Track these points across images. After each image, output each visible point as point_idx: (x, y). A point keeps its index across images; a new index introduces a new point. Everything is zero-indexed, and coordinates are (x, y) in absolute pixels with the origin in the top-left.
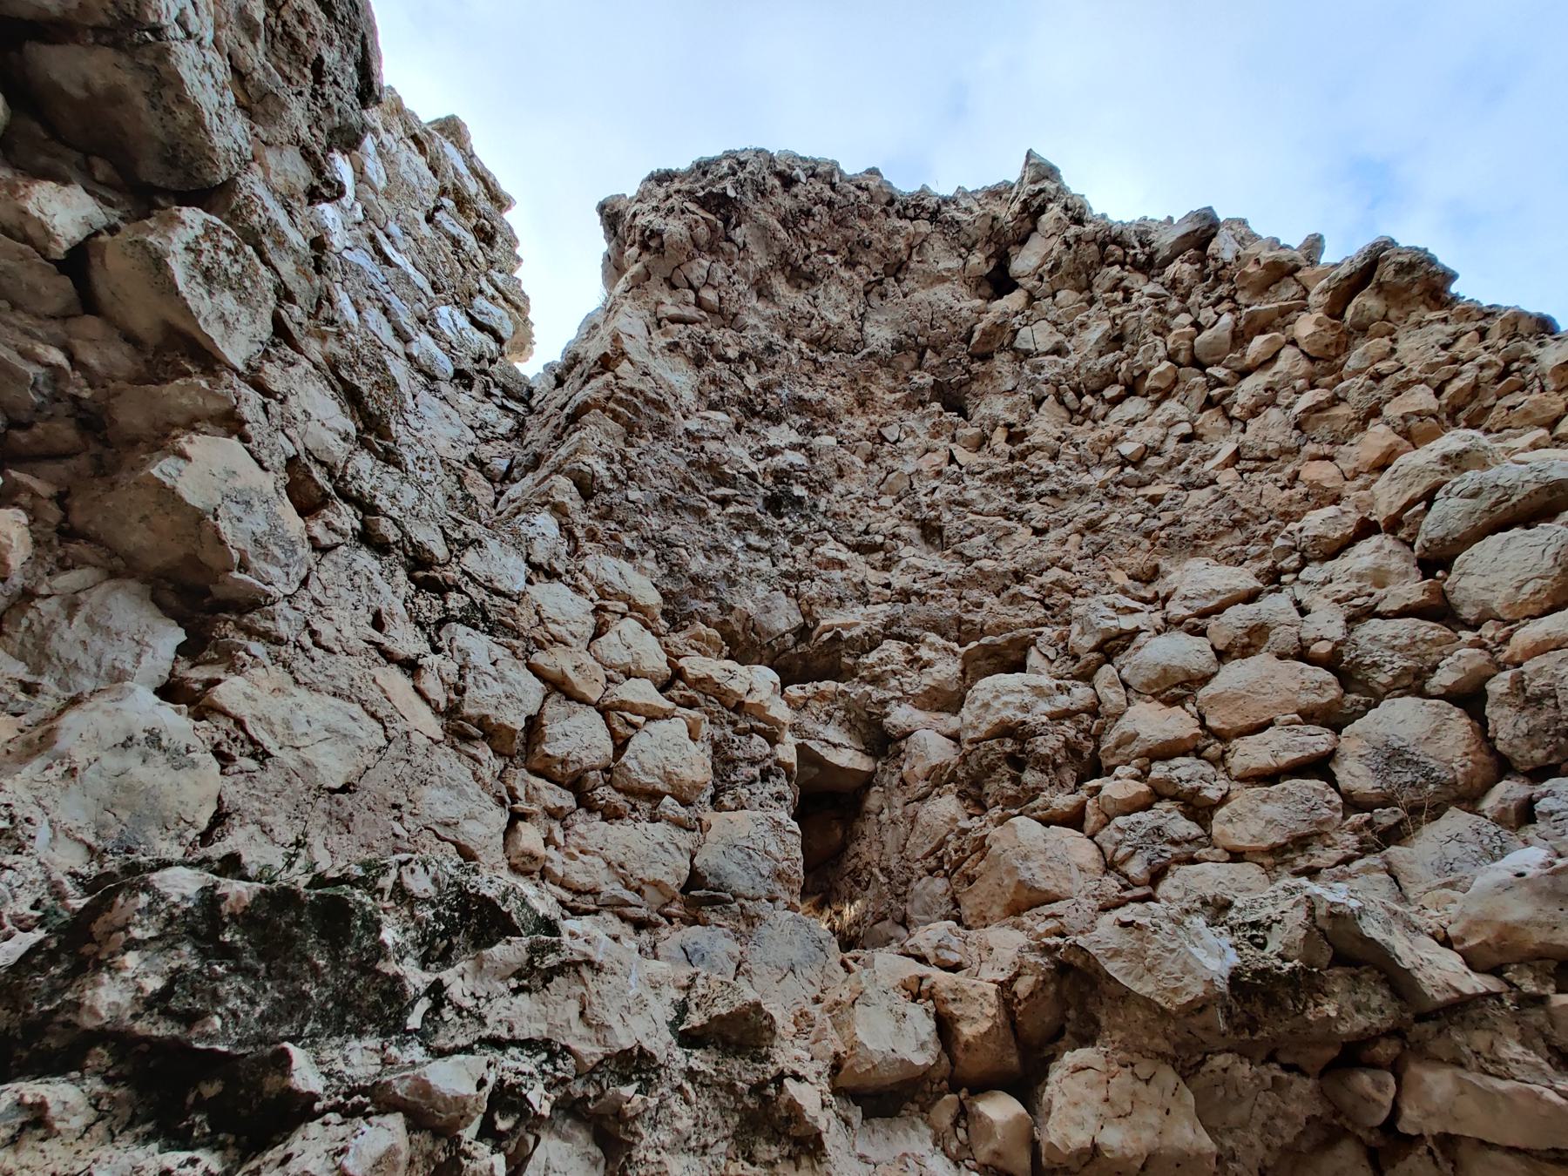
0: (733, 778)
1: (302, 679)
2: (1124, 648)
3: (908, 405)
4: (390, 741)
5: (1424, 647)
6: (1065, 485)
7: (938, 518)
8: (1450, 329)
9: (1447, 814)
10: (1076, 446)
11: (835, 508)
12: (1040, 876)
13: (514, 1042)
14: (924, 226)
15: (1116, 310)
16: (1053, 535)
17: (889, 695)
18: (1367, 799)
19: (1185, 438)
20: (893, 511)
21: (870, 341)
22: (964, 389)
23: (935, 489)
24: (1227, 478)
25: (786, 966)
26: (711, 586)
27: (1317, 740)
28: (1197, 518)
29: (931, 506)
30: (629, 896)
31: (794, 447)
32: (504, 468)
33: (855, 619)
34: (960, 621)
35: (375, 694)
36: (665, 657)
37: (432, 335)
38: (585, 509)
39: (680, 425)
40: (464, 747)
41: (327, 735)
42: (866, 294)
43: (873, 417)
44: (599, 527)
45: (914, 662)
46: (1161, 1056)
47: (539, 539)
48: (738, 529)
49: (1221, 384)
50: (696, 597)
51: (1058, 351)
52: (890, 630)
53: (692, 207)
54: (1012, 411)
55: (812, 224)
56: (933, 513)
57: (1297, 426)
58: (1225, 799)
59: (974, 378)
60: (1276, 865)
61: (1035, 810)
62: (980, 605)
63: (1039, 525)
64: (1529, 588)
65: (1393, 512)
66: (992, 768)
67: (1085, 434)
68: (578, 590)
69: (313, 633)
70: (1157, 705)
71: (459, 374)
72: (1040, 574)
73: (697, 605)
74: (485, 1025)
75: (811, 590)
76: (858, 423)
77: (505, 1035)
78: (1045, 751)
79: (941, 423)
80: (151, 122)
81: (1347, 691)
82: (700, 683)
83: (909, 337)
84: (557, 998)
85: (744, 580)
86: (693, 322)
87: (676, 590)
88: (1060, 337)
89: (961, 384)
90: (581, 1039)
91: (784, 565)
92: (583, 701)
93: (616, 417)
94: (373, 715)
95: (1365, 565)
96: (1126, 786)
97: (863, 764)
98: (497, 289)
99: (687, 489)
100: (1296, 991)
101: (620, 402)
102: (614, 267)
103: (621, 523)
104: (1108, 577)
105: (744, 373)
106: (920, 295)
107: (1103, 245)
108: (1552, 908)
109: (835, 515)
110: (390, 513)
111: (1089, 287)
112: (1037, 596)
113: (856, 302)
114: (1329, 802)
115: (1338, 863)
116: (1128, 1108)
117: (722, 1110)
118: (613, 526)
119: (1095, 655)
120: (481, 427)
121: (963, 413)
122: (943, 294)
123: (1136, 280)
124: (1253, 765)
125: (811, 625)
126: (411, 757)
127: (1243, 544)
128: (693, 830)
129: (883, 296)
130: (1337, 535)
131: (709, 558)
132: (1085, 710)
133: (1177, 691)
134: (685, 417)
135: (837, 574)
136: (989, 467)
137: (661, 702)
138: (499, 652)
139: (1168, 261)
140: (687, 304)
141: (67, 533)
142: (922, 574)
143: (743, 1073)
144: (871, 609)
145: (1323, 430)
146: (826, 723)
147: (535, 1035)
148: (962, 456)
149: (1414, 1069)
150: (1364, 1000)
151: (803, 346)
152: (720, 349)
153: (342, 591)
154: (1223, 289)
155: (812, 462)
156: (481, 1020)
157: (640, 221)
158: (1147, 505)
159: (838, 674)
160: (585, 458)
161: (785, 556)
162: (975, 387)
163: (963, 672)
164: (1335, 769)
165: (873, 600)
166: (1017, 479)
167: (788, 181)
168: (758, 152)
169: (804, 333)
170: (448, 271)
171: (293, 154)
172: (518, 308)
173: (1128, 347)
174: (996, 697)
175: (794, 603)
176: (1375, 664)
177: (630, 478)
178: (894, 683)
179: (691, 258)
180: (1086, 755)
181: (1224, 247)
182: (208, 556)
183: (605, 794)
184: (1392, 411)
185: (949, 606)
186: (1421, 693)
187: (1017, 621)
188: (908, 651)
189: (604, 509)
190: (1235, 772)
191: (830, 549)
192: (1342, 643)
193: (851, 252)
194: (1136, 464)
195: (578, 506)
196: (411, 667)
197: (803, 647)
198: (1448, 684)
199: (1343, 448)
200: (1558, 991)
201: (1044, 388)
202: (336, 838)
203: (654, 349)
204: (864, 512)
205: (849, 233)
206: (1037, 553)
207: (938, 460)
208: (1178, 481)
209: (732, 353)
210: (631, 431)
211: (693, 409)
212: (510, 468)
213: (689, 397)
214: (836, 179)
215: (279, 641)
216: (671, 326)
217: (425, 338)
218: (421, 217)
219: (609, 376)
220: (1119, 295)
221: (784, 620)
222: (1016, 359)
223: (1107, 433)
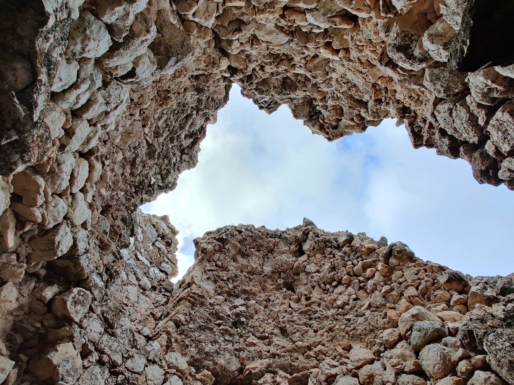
2: (333, 381)
6: (322, 315)
7: (285, 327)
8: (416, 269)
10: (325, 301)
14: (277, 240)
15: (332, 260)
16: (319, 333)
19: (355, 300)
23: (285, 316)
24: (368, 313)
26: (211, 356)
28: (361, 328)
29: (283, 322)
31: (242, 305)
32: (160, 316)
34: (291, 365)
37: (147, 277)
42: (263, 258)
43: (267, 294)
44: (179, 338)
48: (222, 334)
49: (363, 282)
50: (206, 360)
51: (318, 271)
52: (269, 369)
53: (214, 241)
54: (306, 290)
55: (247, 242)
56: (284, 325)
59: (295, 280)
62: (297, 359)
63: (315, 329)
64: (436, 367)
67: (328, 298)
68: (161, 367)
72: (315, 347)
73: (206, 363)
79: (286, 295)
80: (73, 271)
85: (222, 352)
86: (214, 271)
88: (318, 268)
89: (292, 282)
91: (236, 346)
98: (169, 259)
99: (208, 322)
101: (191, 297)
102: (197, 255)
103: (186, 336)
104: (335, 349)
105: (229, 283)
106: (278, 258)
107: (325, 243)
109: (254, 327)
111: (324, 253)
112: (314, 356)
113: (260, 261)
118: (183, 337)
120: (156, 303)
122: (284, 257)
123: (336, 252)
125: (243, 367)
127: (374, 338)
129: (268, 258)
130: (392, 340)
131: (213, 345)
134: (210, 299)
135: (252, 348)
136: (300, 309)
139: (343, 246)
141: (26, 372)
144: (263, 361)
148: (293, 305)
151: (246, 274)
154: (358, 254)
157: (202, 246)
158: (346, 322)
161: (237, 342)
162: (296, 283)
165: (264, 357)
167: (240, 232)
168: (232, 226)
171: (111, 255)
172: (174, 264)
173: (337, 270)
175: (238, 359)
177: (191, 320)
179: (214, 254)
181: (356, 243)
182: (54, 377)
184: (406, 294)
185: (286, 360)
187: (309, 365)
191: (252, 339)
193: (258, 247)
194: (342, 308)
195: (174, 331)
197: (241, 376)
201: (314, 283)
203: (203, 279)
205: (257, 243)
206: (314, 339)
209: (225, 278)
210: (193, 305)
211: (213, 296)
212: (161, 315)
213: (212, 292)
214: (253, 230)
216: (208, 273)
217: (145, 279)
218: (150, 245)
219: (189, 289)
220: (332, 256)
221: (234, 366)
222: (306, 274)
223: (333, 297)
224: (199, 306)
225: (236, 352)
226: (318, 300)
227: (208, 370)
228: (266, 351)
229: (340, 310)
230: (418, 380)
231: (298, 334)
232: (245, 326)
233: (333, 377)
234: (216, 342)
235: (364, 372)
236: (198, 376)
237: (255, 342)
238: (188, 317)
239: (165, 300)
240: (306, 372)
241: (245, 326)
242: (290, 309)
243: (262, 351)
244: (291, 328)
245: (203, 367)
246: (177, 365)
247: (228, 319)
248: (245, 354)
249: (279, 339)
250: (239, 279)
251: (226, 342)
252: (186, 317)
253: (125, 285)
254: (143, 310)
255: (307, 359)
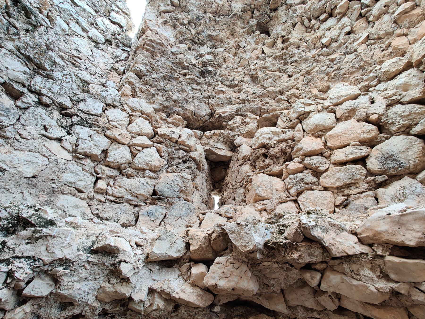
0: (173, 163)
1: (16, 148)
2: (306, 118)
3: (248, 33)
4: (50, 162)
5: (414, 116)
6: (300, 58)
7: (256, 74)
9: (404, 178)
11: (223, 73)
12: (262, 192)
13: (23, 257)
16: (294, 77)
17: (235, 133)
18: (375, 172)
19: (349, 33)
20: (242, 72)
21: (234, 9)
22: (268, 24)
23: (256, 63)
24: (361, 49)
25: (178, 216)
26: (180, 103)
27: (363, 151)
28: (347, 66)
30: (131, 198)
31: (209, 53)
32: (122, 70)
33: (227, 110)
34: (261, 109)
35: (44, 149)
36: (152, 128)
37: (96, 28)
38: (140, 82)
39: (169, 50)
40: (79, 161)
41: (27, 163)
43: (236, 39)
44: (143, 87)
45: (244, 123)
46: (244, 262)
47: (109, 96)
50: (176, 106)
52: (238, 113)
54: (284, 30)
57: (395, 22)
58: (327, 170)
59: (271, 19)
60: (337, 192)
61: (267, 171)
62: (268, 103)
63: (290, 74)
65: (418, 58)
66: (258, 158)
67: (310, 37)
68: (124, 110)
69: (20, 135)
70: (312, 138)
71: (107, 41)
72: (288, 91)
73: (176, 109)
74: (14, 253)
75: (212, 102)
76: (231, 42)
77: (20, 255)
78: (273, 153)
81: (381, 133)
82: (163, 136)
83: (248, 5)
84: (39, 245)
85: (191, 100)
87: (168, 105)
90: (45, 256)
92: (123, 144)
93: (148, 50)
94: (44, 156)
95: (401, 82)
96: (295, 165)
97: (229, 154)
99: (173, 72)
100: (286, 249)
101: (148, 45)
104: (310, 91)
105: (191, 29)
108: (396, 228)
109: (222, 76)
110: (47, 95)
112: (286, 99)
114: (361, 173)
115: (359, 193)
116: (229, 276)
117: (102, 270)
118: (148, 86)
119: (296, 120)
120: (115, 58)
121: (268, 34)
124: (338, 160)
125: (213, 112)
126: (58, 166)
128: (157, 179)
130: (394, 70)
131: (180, 94)
132: (290, 139)
133: (319, 133)
134: (171, 47)
135: (221, 96)
137: (150, 143)
138: (92, 132)
140: (168, 5)
142: (250, 94)
143: (108, 261)
144: (233, 106)
145: (406, 23)
146: (217, 142)
147: (30, 255)
149: (328, 273)
150: (313, 252)
151: (211, 15)
152: (181, 21)
153: (31, 121)
155: (215, 58)
156: (14, 251)
158: (329, 62)
159: (222, 127)
160: (138, 66)
161: (205, 91)
162: (272, 22)
163: (258, 126)
164: (367, 161)
165: (233, 103)
166: (284, 57)
169: (210, 10)
170: (100, 5)
172: (127, 14)
174: (261, 135)
175: (207, 106)
176: (392, 123)
178: (237, 130)
180: (288, 154)
183: (129, 171)
186: (409, 134)
188: (243, 119)
189: (145, 81)
190: (332, 161)
191: (220, 87)
192: (382, 115)
194: (327, 47)
195: (137, 81)
196: (59, 140)
197: (211, 120)
198: (418, 131)
199: (413, 30)
200: (390, 255)
202: (32, 190)
204: (232, 73)
206: (288, 84)
207: (258, 53)
208: (343, 52)
209: (186, 22)
210: (153, 54)
211: (174, 44)
213: (172, 40)
215: (8, 138)
216: (164, 14)
221: (205, 111)
223: (318, 35)
224: (159, 55)
225: (205, 99)
226: (298, 41)
227: (178, 115)
228: (235, 98)
229: (325, 49)
230: (420, 108)
231: (270, 80)
232: (213, 75)
233: (306, 114)
234: (183, 91)
235: (345, 107)
236: (169, 120)
237: (224, 90)
238: (149, 67)
239: (125, 55)
240: (276, 112)
241: (213, 75)
242: (263, 55)
243: (232, 97)
244: (263, 75)
245: (174, 113)
246: (140, 109)
247: (194, 68)
248: (214, 101)
249: (249, 86)
250: (203, 21)
251: (194, 91)
252: (147, 67)
253: (68, 35)
254: (102, 65)
255: (278, 102)
